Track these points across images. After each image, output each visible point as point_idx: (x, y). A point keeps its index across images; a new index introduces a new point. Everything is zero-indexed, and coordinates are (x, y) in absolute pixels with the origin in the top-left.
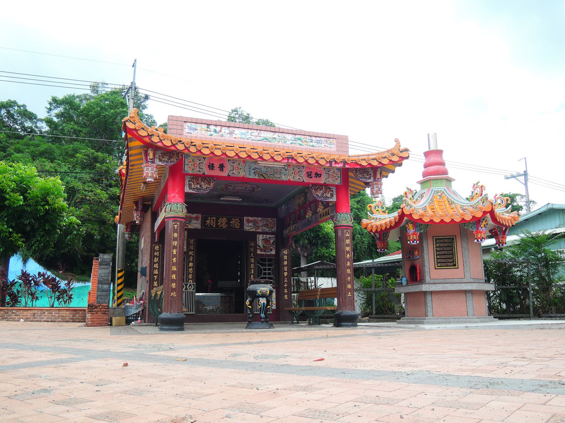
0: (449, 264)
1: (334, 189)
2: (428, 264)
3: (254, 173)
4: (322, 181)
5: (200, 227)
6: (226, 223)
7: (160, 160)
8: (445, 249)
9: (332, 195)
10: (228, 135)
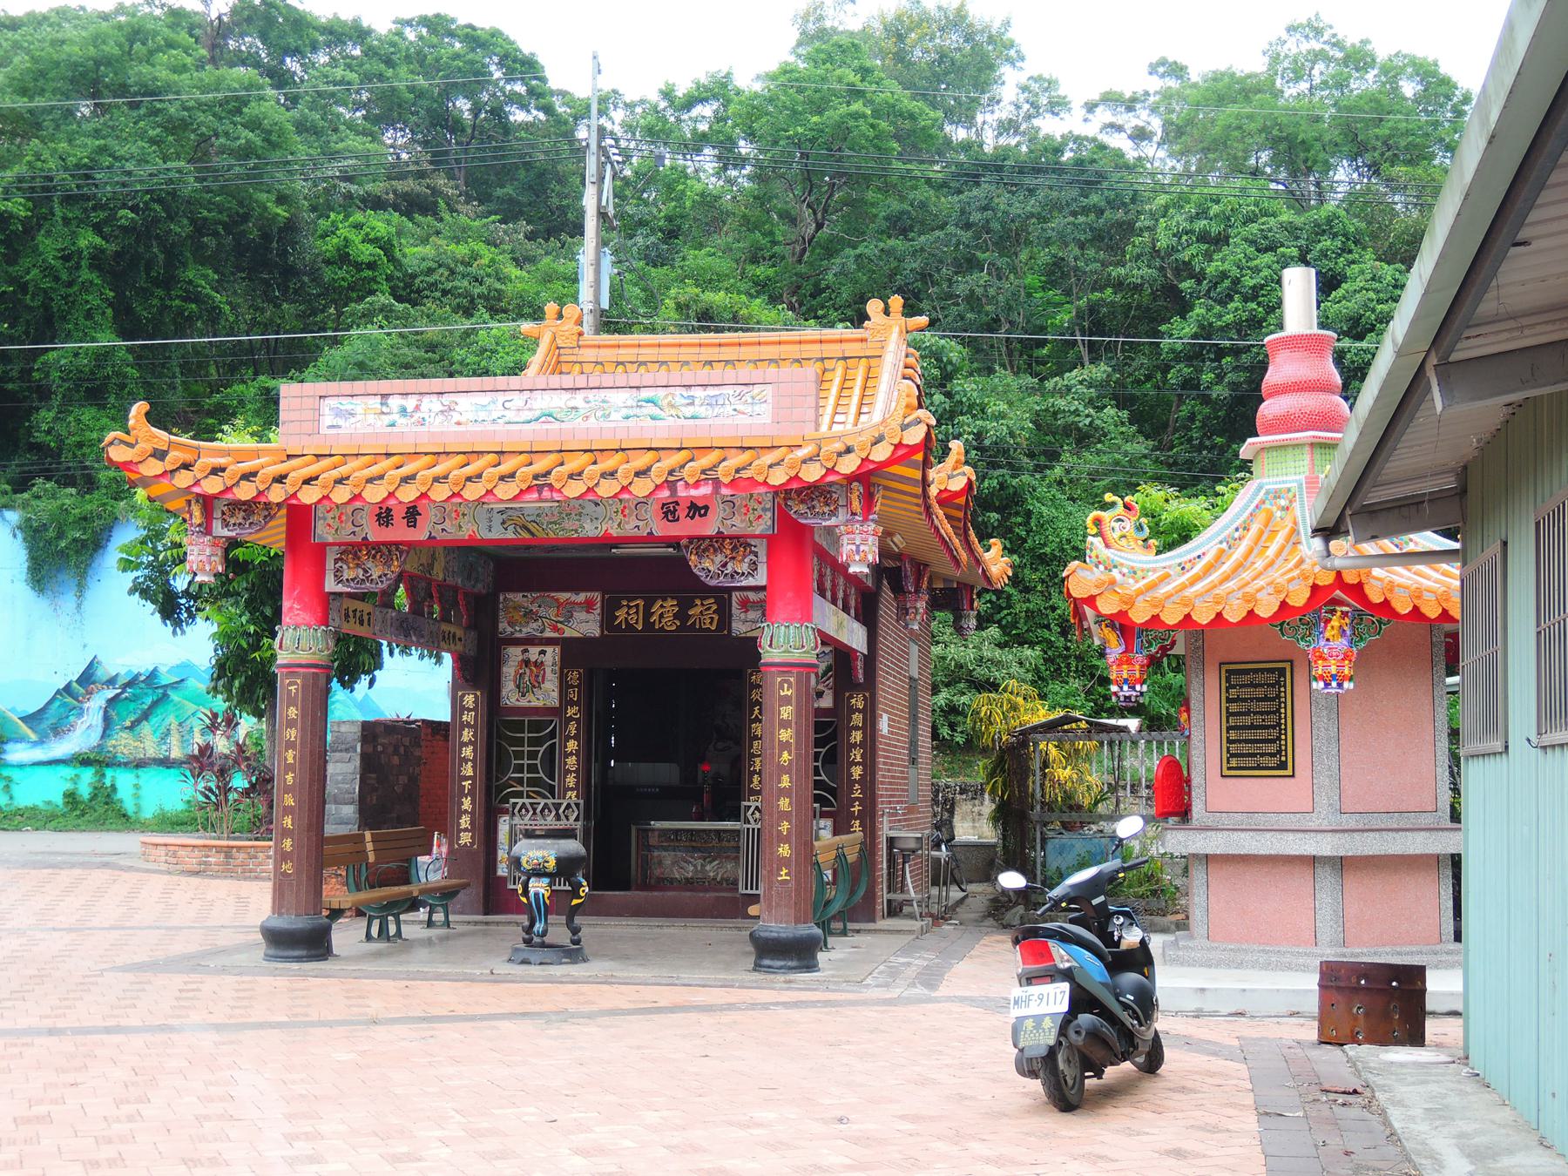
0: (1265, 761)
1: (762, 549)
2: (1201, 760)
4: (710, 526)
5: (597, 633)
6: (676, 616)
7: (226, 525)
8: (1254, 706)
9: (754, 566)
10: (440, 418)
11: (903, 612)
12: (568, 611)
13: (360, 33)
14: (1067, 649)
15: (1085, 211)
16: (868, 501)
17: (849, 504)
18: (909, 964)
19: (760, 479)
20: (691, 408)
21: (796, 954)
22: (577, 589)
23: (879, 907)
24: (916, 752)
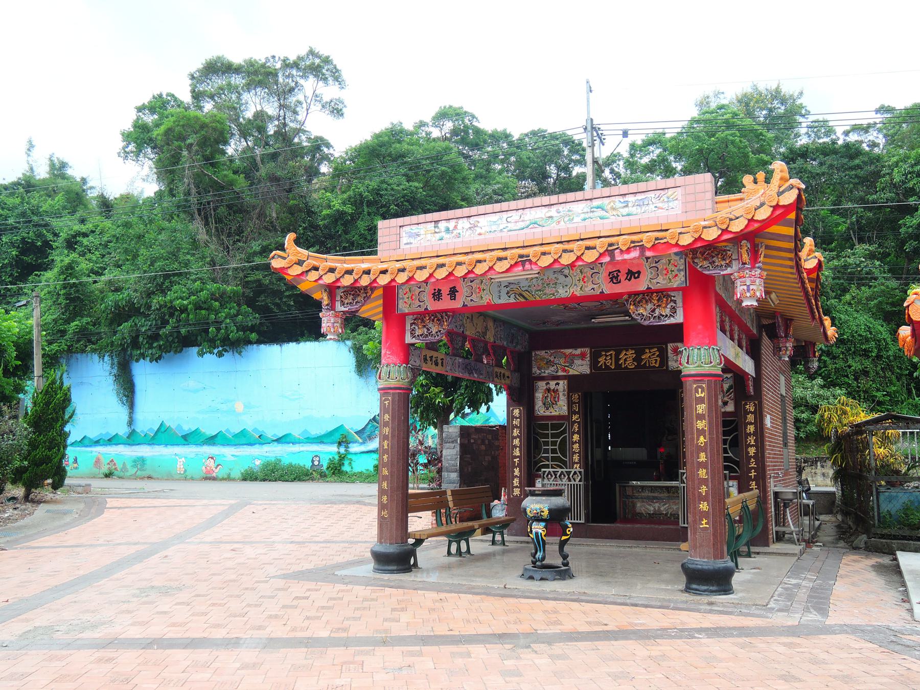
3: (508, 293)
4: (642, 285)
6: (634, 360)
7: (343, 304)
9: (674, 311)
11: (777, 350)
12: (571, 360)
13: (506, 136)
14: (859, 387)
15: (851, 168)
16: (754, 255)
17: (740, 256)
18: (798, 586)
19: (673, 242)
20: (626, 209)
21: (714, 581)
22: (575, 347)
23: (771, 537)
24: (787, 439)
